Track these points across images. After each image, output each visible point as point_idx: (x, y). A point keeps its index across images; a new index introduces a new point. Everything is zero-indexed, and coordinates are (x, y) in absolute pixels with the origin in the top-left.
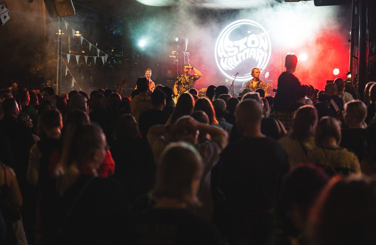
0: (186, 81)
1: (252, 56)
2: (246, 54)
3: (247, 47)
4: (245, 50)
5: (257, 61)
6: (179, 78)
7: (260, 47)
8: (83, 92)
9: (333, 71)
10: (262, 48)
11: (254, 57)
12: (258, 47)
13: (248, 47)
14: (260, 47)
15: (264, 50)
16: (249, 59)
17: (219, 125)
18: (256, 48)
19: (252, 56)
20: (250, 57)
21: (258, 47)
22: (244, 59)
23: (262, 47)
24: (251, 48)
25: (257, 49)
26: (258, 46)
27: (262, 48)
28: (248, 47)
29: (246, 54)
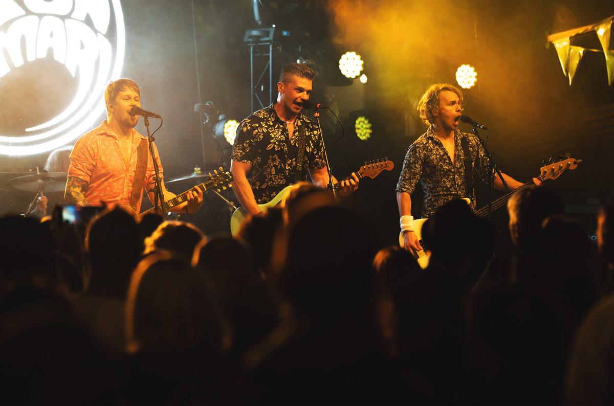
0: (287, 140)
1: (50, 51)
2: (23, 40)
3: (23, 12)
4: (75, 20)
5: (73, 75)
6: (253, 129)
7: (79, 14)
8: (607, 62)
9: (362, 62)
10: (88, 21)
11: (58, 57)
12: (68, 16)
13: (28, 12)
14: (79, 14)
15: (96, 31)
16: (39, 62)
17: (592, 29)
18: (63, 18)
19: (50, 51)
20: (42, 55)
21: (68, 16)
22: (19, 62)
23: (88, 14)
24: (41, 16)
25: (67, 21)
26: (69, 11)
27: (88, 21)
28: (28, 12)
29: (23, 40)
